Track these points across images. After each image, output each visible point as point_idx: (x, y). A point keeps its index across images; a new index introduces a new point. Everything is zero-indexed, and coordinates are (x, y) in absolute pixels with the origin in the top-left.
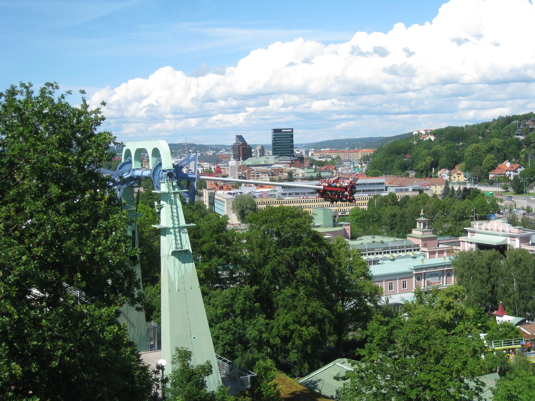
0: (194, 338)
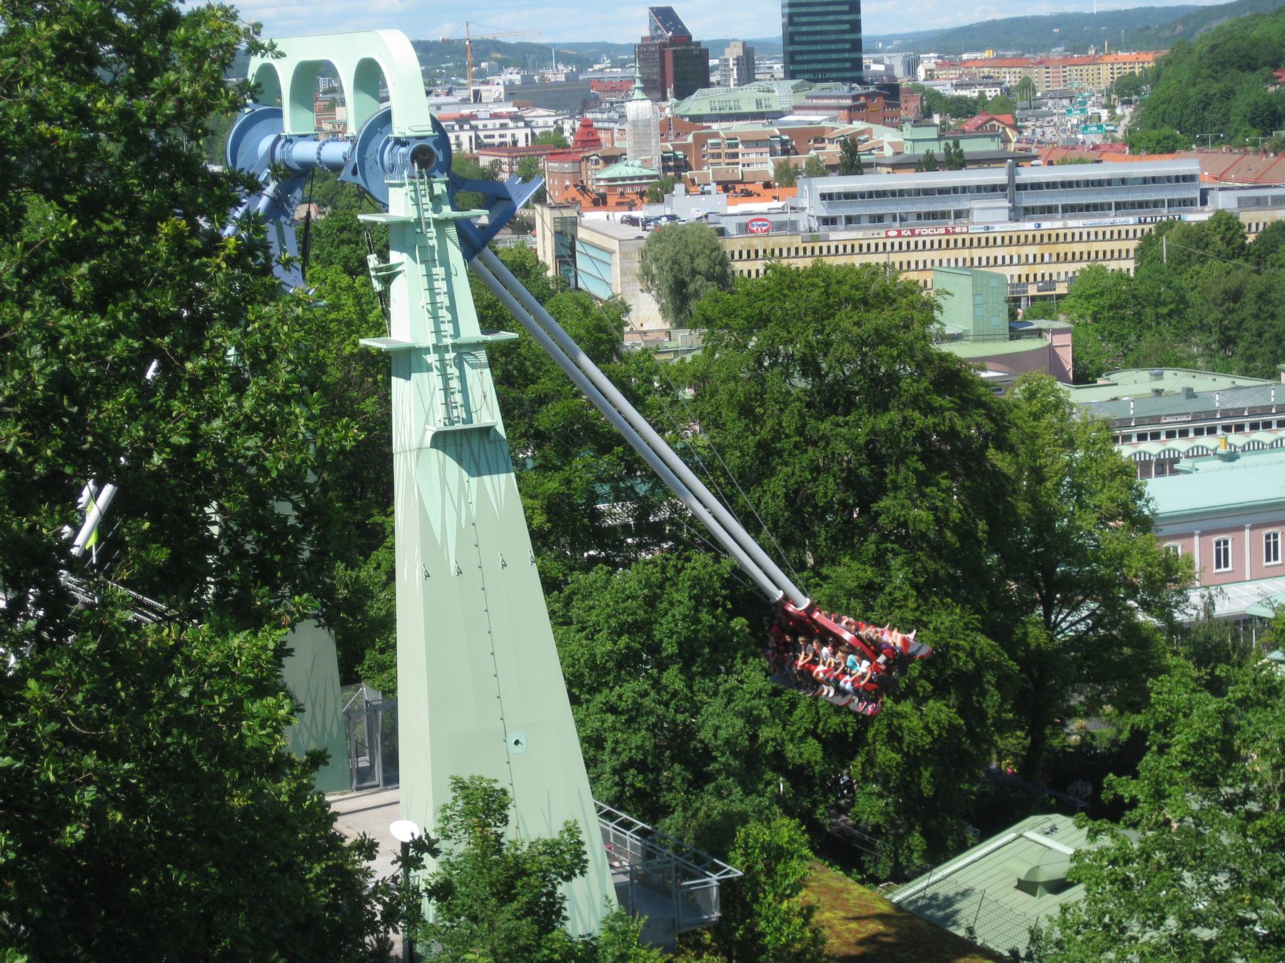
0: (517, 742)
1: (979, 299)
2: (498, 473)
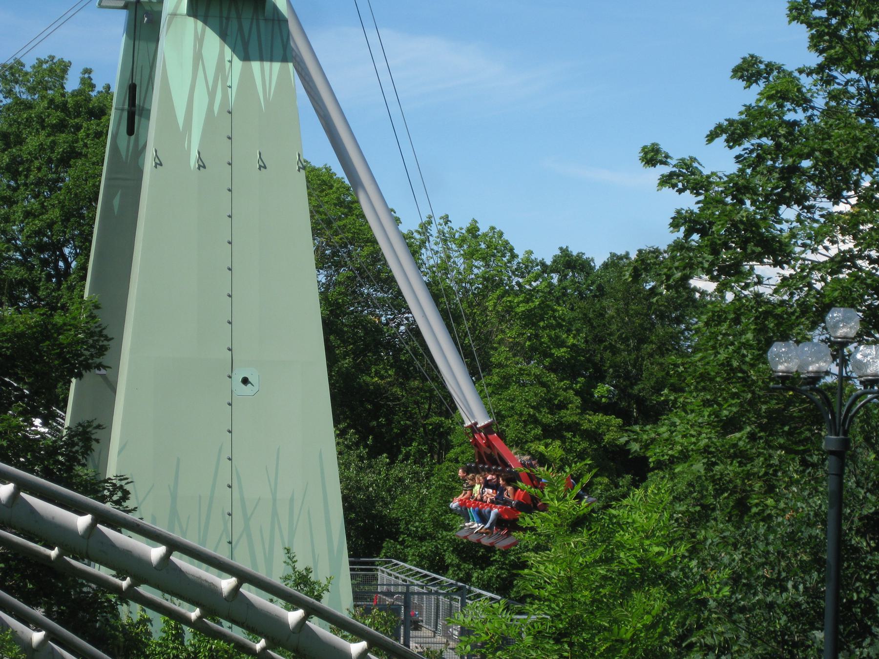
0: (245, 381)
1: (362, 253)
2: (271, 60)
